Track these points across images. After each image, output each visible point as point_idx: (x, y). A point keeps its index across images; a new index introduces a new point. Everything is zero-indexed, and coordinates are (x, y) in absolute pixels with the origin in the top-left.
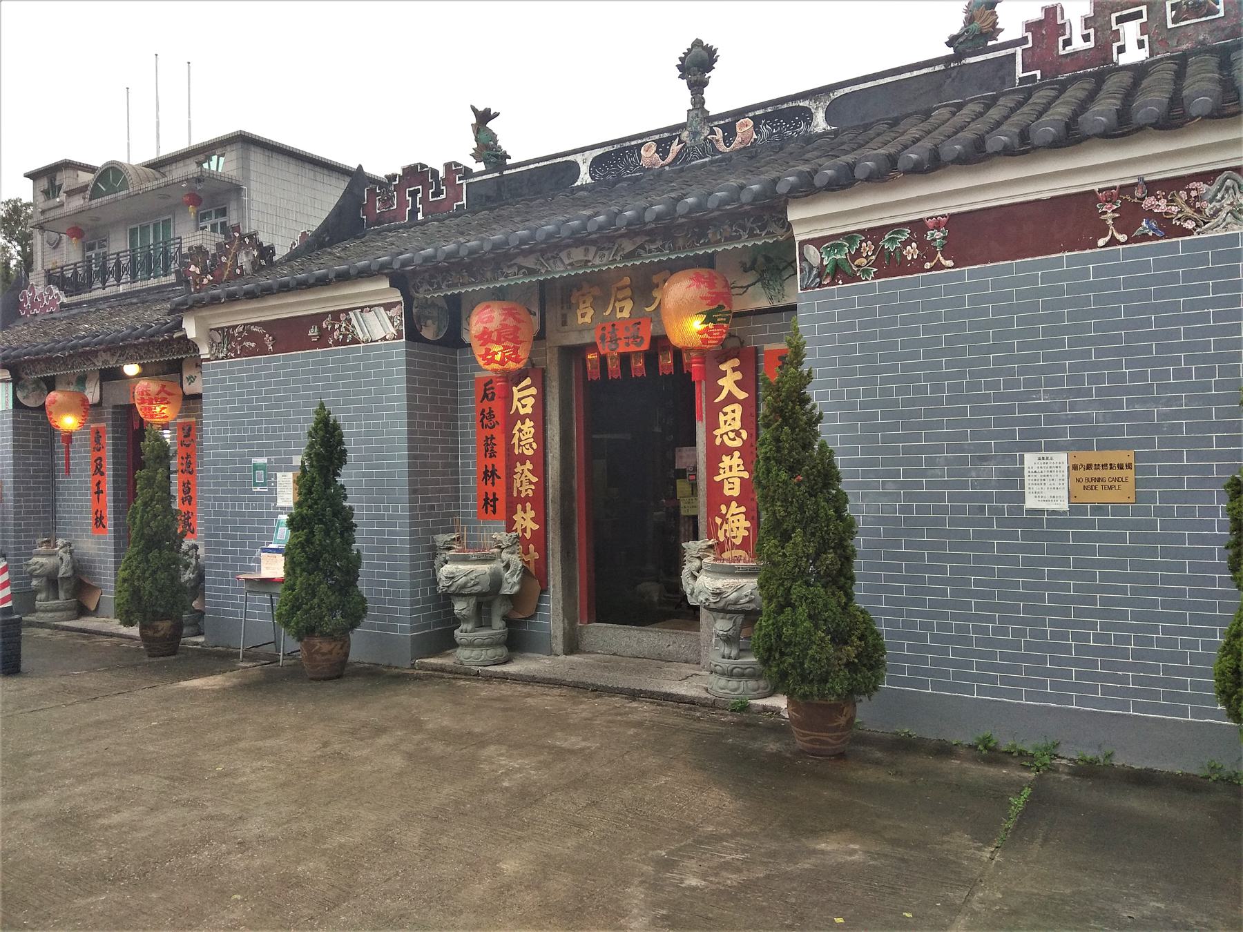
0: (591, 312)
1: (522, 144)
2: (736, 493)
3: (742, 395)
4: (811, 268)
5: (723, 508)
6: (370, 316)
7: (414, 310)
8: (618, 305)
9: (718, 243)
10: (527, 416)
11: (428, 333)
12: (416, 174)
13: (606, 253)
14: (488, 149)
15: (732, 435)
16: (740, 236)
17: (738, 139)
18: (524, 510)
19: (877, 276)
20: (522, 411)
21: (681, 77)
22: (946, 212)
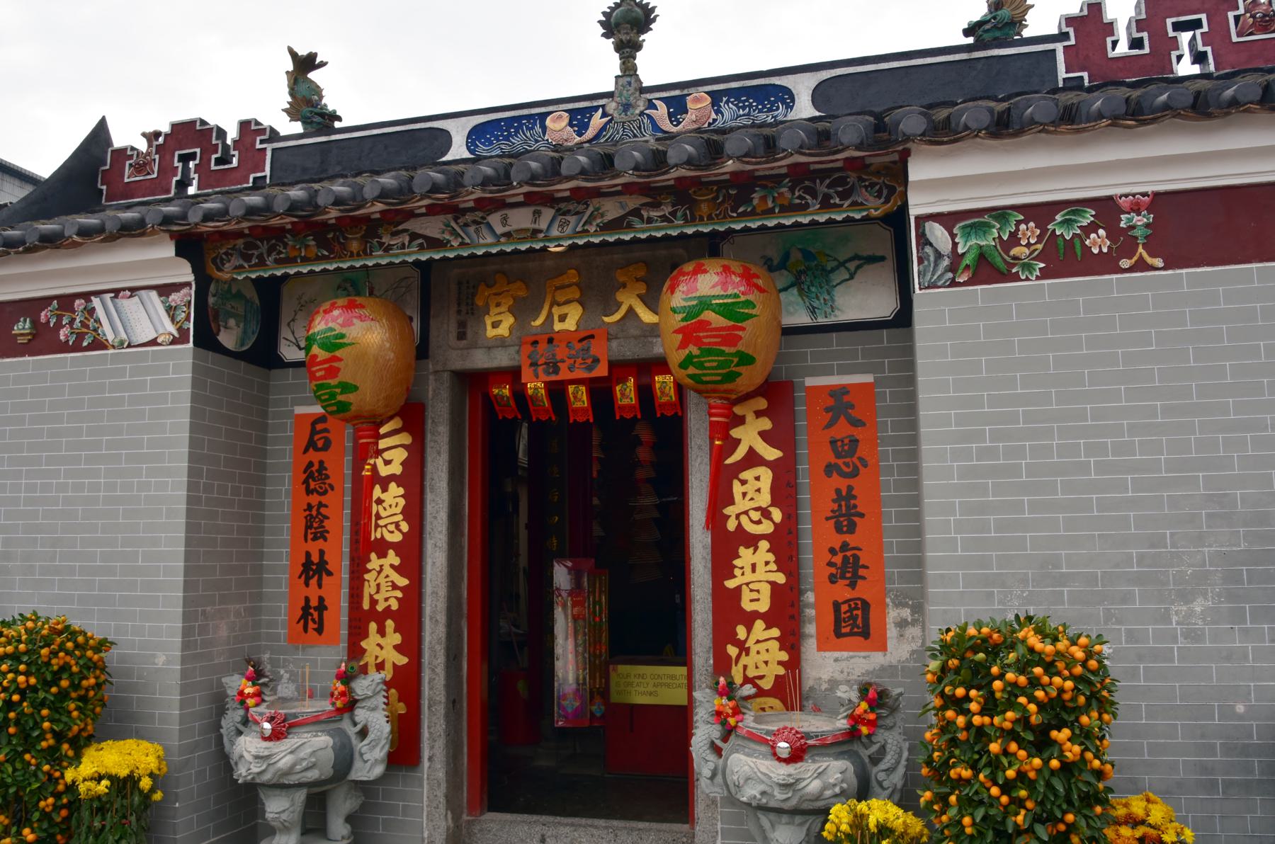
0: (508, 321)
1: (357, 101)
2: (764, 606)
3: (771, 454)
4: (939, 256)
5: (741, 632)
6: (131, 306)
7: (211, 300)
8: (556, 311)
9: (769, 213)
10: (392, 478)
11: (228, 339)
12: (191, 136)
13: (572, 219)
14: (306, 103)
15: (756, 516)
16: (807, 206)
17: (691, 116)
18: (382, 632)
19: (1045, 274)
20: (384, 471)
21: (606, 35)
22: (1149, 189)
